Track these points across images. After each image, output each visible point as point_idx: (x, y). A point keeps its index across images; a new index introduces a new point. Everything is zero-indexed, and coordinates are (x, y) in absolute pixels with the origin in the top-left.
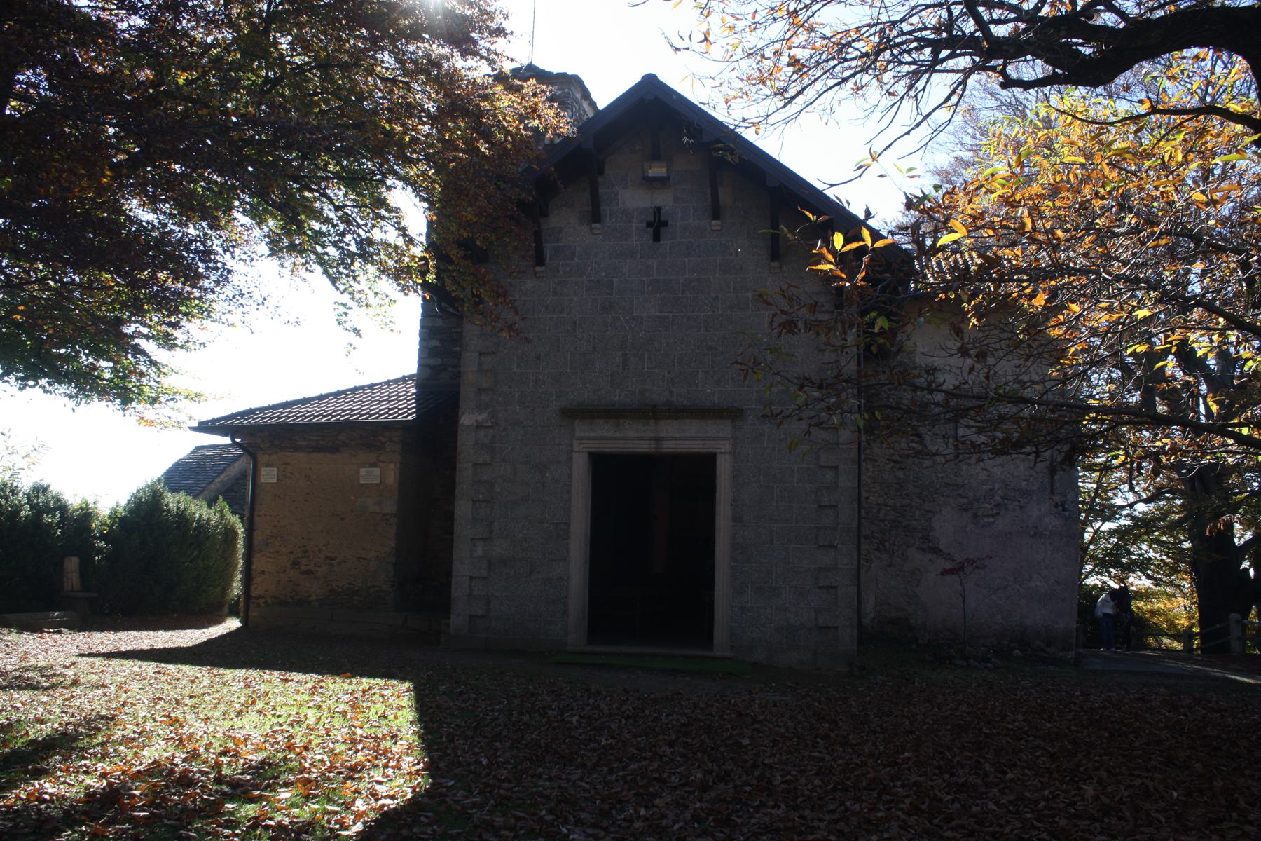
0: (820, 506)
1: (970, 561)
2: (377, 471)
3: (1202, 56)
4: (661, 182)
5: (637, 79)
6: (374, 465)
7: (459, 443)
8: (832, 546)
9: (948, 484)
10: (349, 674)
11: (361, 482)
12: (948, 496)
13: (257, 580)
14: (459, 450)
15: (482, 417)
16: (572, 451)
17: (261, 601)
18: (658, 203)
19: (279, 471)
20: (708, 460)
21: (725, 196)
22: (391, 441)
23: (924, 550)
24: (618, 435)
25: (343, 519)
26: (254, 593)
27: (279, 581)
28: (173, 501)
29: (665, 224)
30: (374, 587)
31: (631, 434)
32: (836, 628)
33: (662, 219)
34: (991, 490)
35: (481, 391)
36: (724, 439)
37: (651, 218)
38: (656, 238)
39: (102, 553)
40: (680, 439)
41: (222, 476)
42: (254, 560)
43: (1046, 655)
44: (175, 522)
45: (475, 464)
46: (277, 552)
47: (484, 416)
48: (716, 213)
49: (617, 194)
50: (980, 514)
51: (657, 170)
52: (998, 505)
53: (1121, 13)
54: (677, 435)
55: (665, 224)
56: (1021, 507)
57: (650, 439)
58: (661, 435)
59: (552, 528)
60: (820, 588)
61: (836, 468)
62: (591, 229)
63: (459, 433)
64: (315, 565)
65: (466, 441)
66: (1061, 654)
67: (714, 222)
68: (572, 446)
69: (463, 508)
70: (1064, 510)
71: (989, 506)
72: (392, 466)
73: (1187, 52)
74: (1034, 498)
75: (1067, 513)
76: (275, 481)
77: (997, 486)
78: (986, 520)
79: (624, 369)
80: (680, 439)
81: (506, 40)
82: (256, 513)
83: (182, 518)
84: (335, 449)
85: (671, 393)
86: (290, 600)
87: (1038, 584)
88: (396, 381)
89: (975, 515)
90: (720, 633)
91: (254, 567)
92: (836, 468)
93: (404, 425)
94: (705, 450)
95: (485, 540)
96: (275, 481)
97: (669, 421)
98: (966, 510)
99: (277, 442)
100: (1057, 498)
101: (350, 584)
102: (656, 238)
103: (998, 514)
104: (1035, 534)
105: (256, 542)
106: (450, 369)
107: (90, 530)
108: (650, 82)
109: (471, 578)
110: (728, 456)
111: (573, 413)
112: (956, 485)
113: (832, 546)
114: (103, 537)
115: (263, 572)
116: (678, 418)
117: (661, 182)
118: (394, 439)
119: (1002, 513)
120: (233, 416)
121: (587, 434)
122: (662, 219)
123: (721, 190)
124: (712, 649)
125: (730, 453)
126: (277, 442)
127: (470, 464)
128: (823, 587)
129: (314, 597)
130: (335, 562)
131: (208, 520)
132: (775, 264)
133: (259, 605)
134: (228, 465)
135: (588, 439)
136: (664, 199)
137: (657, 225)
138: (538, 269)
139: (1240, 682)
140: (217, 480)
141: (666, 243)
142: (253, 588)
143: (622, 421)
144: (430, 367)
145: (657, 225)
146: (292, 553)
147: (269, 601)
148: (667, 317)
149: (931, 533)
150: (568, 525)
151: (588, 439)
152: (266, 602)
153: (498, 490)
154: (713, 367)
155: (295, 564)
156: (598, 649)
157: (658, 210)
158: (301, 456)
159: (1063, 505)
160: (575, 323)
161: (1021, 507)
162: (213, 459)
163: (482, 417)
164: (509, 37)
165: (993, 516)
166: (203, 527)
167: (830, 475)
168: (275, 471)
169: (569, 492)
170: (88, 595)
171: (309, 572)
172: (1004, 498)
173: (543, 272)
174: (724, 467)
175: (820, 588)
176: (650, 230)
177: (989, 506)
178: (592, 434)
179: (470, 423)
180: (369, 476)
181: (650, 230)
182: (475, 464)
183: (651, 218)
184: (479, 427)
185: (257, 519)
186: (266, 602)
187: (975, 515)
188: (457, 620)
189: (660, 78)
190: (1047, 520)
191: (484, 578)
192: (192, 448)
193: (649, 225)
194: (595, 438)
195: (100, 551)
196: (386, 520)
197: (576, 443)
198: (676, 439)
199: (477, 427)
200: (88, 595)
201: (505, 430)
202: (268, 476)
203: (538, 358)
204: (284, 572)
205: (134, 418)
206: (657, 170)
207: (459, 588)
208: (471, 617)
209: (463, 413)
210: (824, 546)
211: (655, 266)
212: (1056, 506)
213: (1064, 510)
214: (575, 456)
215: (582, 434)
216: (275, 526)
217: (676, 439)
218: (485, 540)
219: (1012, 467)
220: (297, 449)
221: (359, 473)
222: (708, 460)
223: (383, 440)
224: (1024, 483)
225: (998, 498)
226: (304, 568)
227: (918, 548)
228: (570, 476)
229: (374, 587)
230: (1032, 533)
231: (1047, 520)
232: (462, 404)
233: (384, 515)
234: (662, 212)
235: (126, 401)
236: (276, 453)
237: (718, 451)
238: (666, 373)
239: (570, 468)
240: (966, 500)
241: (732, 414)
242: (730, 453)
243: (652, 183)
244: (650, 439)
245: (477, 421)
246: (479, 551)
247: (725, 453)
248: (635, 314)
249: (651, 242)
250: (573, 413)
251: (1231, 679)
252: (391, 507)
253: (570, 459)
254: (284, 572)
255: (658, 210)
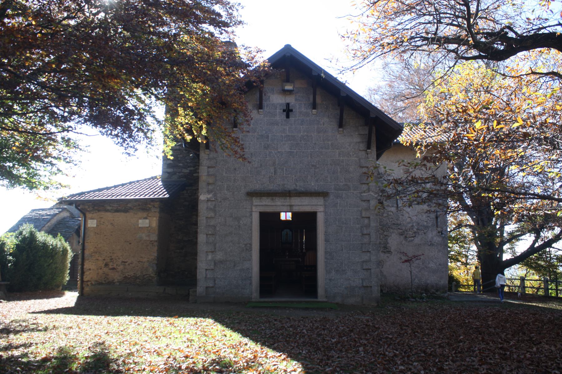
0: (363, 234)
1: (415, 257)
2: (147, 221)
3: (542, 51)
4: (290, 92)
5: (282, 46)
6: (146, 218)
7: (199, 208)
8: (368, 251)
9: (394, 224)
10: (177, 316)
11: (140, 226)
12: (394, 229)
13: (87, 273)
14: (199, 211)
15: (209, 196)
16: (252, 211)
17: (89, 283)
18: (288, 101)
19: (97, 221)
20: (313, 215)
21: (318, 100)
22: (154, 207)
23: (385, 252)
24: (273, 204)
25: (130, 244)
26: (85, 279)
27: (98, 273)
28: (41, 236)
29: (292, 111)
30: (146, 275)
31: (279, 203)
32: (371, 287)
33: (290, 108)
34: (412, 226)
35: (209, 184)
36: (321, 205)
37: (285, 108)
38: (288, 116)
39: (11, 262)
40: (301, 205)
41: (49, 224)
42: (85, 263)
43: (436, 295)
44: (42, 246)
45: (207, 218)
46: (98, 260)
47: (210, 196)
48: (314, 106)
49: (269, 97)
50: (408, 236)
51: (288, 87)
52: (415, 233)
53: (516, 33)
54: (300, 204)
55: (292, 111)
56: (425, 233)
57: (287, 206)
58: (293, 204)
59: (243, 246)
60: (364, 269)
61: (369, 218)
62: (258, 112)
63: (199, 203)
64: (117, 265)
65: (202, 208)
66: (442, 295)
67: (314, 111)
68: (252, 209)
69: (202, 238)
70: (442, 234)
71: (411, 233)
72: (155, 218)
73: (537, 50)
74: (430, 229)
75: (443, 235)
76: (95, 226)
77: (414, 224)
78: (410, 239)
79: (275, 174)
80: (301, 205)
81: (242, 27)
82: (86, 241)
83: (45, 245)
84: (126, 211)
85: (296, 185)
86: (104, 282)
87: (432, 265)
88: (149, 179)
89: (406, 237)
90: (321, 291)
91: (85, 267)
92: (369, 218)
93: (162, 201)
94: (312, 211)
95: (212, 252)
96: (95, 226)
97: (296, 198)
98: (402, 235)
99: (96, 208)
100: (439, 229)
101: (134, 274)
102: (288, 116)
103: (415, 236)
104: (431, 244)
105: (86, 255)
106: (178, 174)
107: (4, 251)
108: (288, 48)
109: (206, 270)
110: (322, 213)
111: (252, 194)
112: (397, 224)
113: (368, 251)
114: (11, 254)
115: (90, 269)
116: (299, 196)
117: (290, 92)
118: (155, 206)
119: (417, 236)
120: (73, 196)
121: (259, 204)
122: (290, 108)
123: (317, 96)
124: (316, 297)
125: (323, 212)
126: (96, 208)
127: (204, 218)
128: (365, 269)
129: (116, 281)
130: (127, 264)
131: (56, 245)
132: (341, 129)
133: (88, 285)
134: (52, 218)
135: (260, 206)
136: (291, 99)
137: (288, 111)
138: (235, 129)
139: (514, 303)
140: (46, 226)
141: (292, 119)
142: (85, 277)
143: (274, 198)
144: (168, 173)
145: (288, 111)
146: (104, 260)
147: (93, 283)
148: (294, 152)
149: (388, 245)
150: (251, 244)
151: (260, 206)
152: (91, 284)
153: (218, 229)
154: (314, 174)
155: (106, 265)
156: (266, 300)
157: (288, 105)
158: (108, 214)
159: (441, 232)
160: (252, 154)
161: (425, 233)
162: (43, 216)
163: (209, 196)
164: (244, 25)
165: (413, 237)
166: (54, 248)
167: (366, 221)
168: (95, 221)
169: (251, 230)
170: (6, 283)
171: (114, 269)
172: (417, 229)
173: (237, 131)
174: (320, 218)
175: (364, 269)
176: (285, 113)
177: (411, 233)
178: (261, 204)
179: (204, 199)
180: (143, 223)
181: (285, 113)
182: (207, 218)
183: (285, 108)
184: (208, 200)
185: (86, 244)
186: (91, 284)
187: (406, 237)
188: (200, 289)
189: (293, 46)
190: (435, 238)
191: (212, 269)
192: (30, 210)
193: (284, 111)
194: (262, 206)
195: (10, 261)
196: (152, 244)
197: (254, 208)
198: (299, 206)
199: (208, 200)
200: (6, 283)
201: (220, 202)
202: (92, 224)
203: (235, 169)
204: (101, 269)
205: (36, 196)
206: (288, 87)
207: (201, 274)
208: (207, 288)
209: (201, 195)
210: (365, 252)
211: (287, 129)
212: (439, 232)
213: (442, 234)
214: (253, 213)
215: (256, 204)
216: (95, 247)
217: (299, 206)
218: (212, 252)
219: (421, 216)
220: (107, 211)
221: (138, 222)
222: (313, 215)
223: (150, 206)
224: (426, 223)
225: (415, 230)
226: (111, 267)
227: (382, 252)
228: (251, 223)
229: (146, 275)
230: (429, 244)
231: (435, 238)
232: (200, 190)
233: (151, 241)
234: (290, 105)
235: (31, 188)
236: (96, 213)
237: (318, 211)
238: (294, 176)
239: (251, 219)
240: (402, 231)
241: (323, 194)
242: (323, 212)
243: (285, 92)
244: (287, 206)
245: (207, 198)
246: (210, 257)
247: (321, 212)
248: (279, 150)
249: (285, 118)
250: (252, 194)
251: (530, 305)
252: (154, 237)
253: (251, 215)
254: (101, 269)
255: (288, 105)
